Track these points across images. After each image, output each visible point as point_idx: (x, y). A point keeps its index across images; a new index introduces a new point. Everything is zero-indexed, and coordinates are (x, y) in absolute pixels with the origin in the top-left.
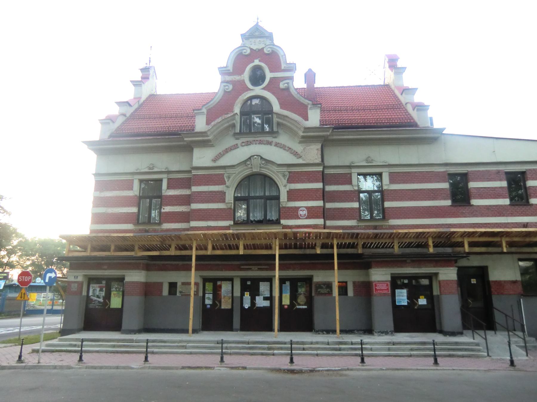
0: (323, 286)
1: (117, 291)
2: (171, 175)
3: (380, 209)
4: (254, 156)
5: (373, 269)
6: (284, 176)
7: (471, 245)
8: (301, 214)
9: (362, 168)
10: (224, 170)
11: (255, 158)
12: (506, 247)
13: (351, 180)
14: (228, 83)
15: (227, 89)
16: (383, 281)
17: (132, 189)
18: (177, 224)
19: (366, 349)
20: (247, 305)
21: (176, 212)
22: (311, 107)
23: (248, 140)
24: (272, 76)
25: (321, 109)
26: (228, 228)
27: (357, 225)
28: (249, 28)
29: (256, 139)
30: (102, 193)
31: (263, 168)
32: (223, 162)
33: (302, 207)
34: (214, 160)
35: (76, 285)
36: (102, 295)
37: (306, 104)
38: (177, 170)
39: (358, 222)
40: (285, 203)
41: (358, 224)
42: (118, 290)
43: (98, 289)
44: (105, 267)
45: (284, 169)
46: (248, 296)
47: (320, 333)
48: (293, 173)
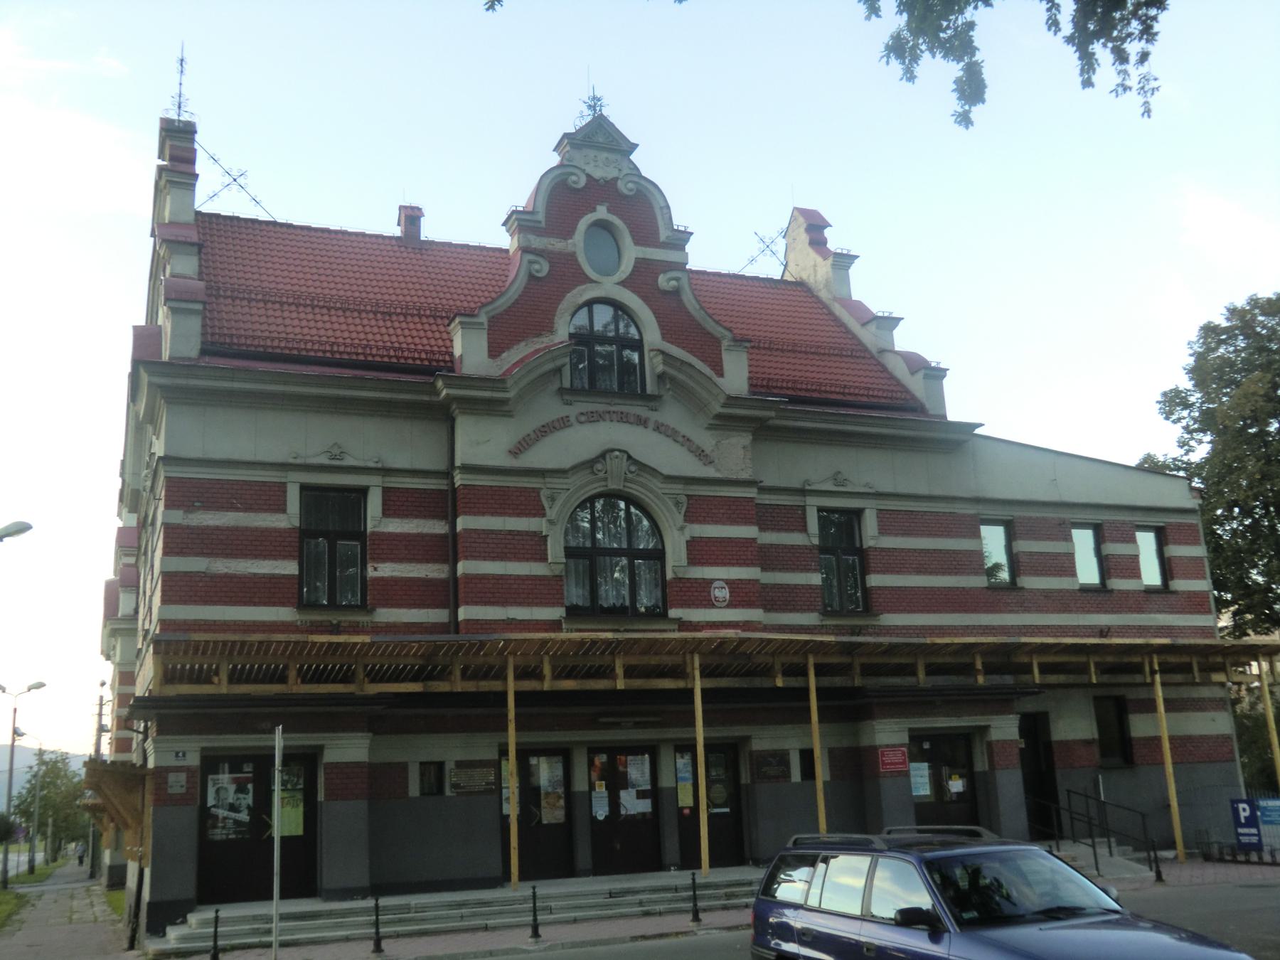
0: (771, 759)
2: (393, 479)
4: (613, 450)
6: (677, 504)
7: (1045, 669)
8: (717, 595)
9: (852, 498)
10: (541, 480)
11: (617, 457)
12: (1096, 674)
13: (806, 522)
14: (542, 256)
15: (538, 271)
16: (894, 746)
17: (284, 511)
18: (414, 611)
19: (703, 897)
22: (729, 346)
23: (594, 410)
24: (641, 256)
25: (204, 318)
26: (555, 626)
27: (819, 623)
28: (614, 123)
30: (190, 516)
31: (631, 481)
32: (540, 457)
34: (515, 452)
35: (183, 777)
36: (244, 803)
39: (821, 617)
41: (822, 620)
42: (289, 786)
45: (678, 488)
46: (604, 789)
48: (694, 498)
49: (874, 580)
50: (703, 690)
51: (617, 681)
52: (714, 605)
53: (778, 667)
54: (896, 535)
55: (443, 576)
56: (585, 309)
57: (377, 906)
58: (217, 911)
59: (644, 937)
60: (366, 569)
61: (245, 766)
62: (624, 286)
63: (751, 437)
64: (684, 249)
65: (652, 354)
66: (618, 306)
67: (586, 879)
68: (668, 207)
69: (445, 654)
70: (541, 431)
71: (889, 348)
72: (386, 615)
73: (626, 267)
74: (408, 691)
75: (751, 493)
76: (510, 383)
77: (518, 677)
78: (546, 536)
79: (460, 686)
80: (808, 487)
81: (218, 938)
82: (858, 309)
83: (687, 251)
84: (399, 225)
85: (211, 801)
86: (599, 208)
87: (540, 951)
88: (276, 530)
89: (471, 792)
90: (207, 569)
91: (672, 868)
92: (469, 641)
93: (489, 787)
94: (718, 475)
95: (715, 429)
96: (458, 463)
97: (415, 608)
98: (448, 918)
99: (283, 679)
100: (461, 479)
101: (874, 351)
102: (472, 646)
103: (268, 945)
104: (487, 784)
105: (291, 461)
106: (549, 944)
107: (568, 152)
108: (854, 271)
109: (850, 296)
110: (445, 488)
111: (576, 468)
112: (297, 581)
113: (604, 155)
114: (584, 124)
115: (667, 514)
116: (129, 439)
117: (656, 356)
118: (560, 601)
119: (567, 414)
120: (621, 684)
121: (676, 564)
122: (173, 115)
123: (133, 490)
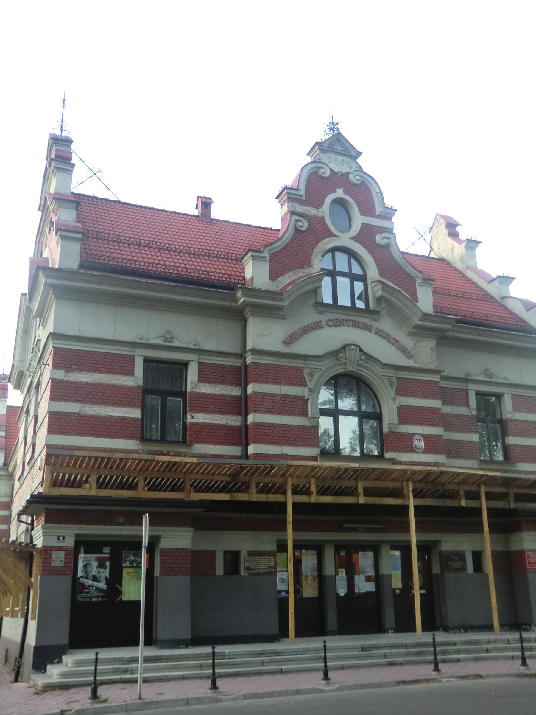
0: (454, 557)
1: (133, 567)
2: (205, 357)
3: (180, 427)
4: (351, 345)
5: (525, 533)
6: (391, 383)
11: (353, 349)
15: (301, 226)
17: (132, 374)
20: (342, 590)
21: (216, 425)
22: (421, 283)
26: (315, 459)
29: (349, 318)
30: (69, 374)
33: (418, 434)
34: (288, 342)
35: (62, 554)
37: (414, 276)
38: (215, 349)
40: (395, 426)
41: (480, 465)
43: (95, 564)
44: (121, 520)
45: (391, 372)
47: (456, 631)
49: (512, 440)
50: (415, 507)
51: (360, 498)
52: (415, 451)
53: (462, 493)
54: (524, 412)
55: (238, 424)
56: (330, 254)
57: (213, 653)
58: (97, 654)
59: (404, 682)
60: (186, 417)
61: (105, 548)
62: (355, 240)
63: (435, 342)
64: (391, 220)
65: (373, 284)
66: (351, 254)
67: (333, 637)
68: (381, 193)
69: (245, 474)
70: (303, 330)
71: (508, 295)
72: (200, 448)
73: (356, 228)
74: (219, 499)
75: (436, 378)
76: (285, 296)
77: (295, 492)
78: (308, 400)
79: (256, 497)
80: (469, 378)
81: (97, 675)
82: (482, 274)
83: (393, 221)
84: (196, 208)
85: (80, 574)
86: (338, 190)
87: (333, 691)
88: (126, 387)
89: (259, 573)
90: (79, 411)
91: (390, 631)
92: (264, 465)
93: (270, 570)
94: (416, 365)
95: (414, 335)
96: (249, 347)
97: (219, 445)
98: (254, 664)
99: (133, 487)
100: (252, 358)
101: (498, 298)
102: (266, 468)
103: (135, 681)
104: (269, 567)
105: (138, 341)
106: (338, 686)
107: (318, 154)
108: (479, 251)
109: (477, 266)
110: (239, 365)
111: (327, 355)
112: (140, 423)
113: (340, 158)
114: (327, 138)
115: (384, 389)
116: (18, 339)
117: (376, 286)
118: (316, 443)
119: (320, 319)
120: (362, 500)
121: (391, 422)
122: (58, 132)
123: (19, 372)
